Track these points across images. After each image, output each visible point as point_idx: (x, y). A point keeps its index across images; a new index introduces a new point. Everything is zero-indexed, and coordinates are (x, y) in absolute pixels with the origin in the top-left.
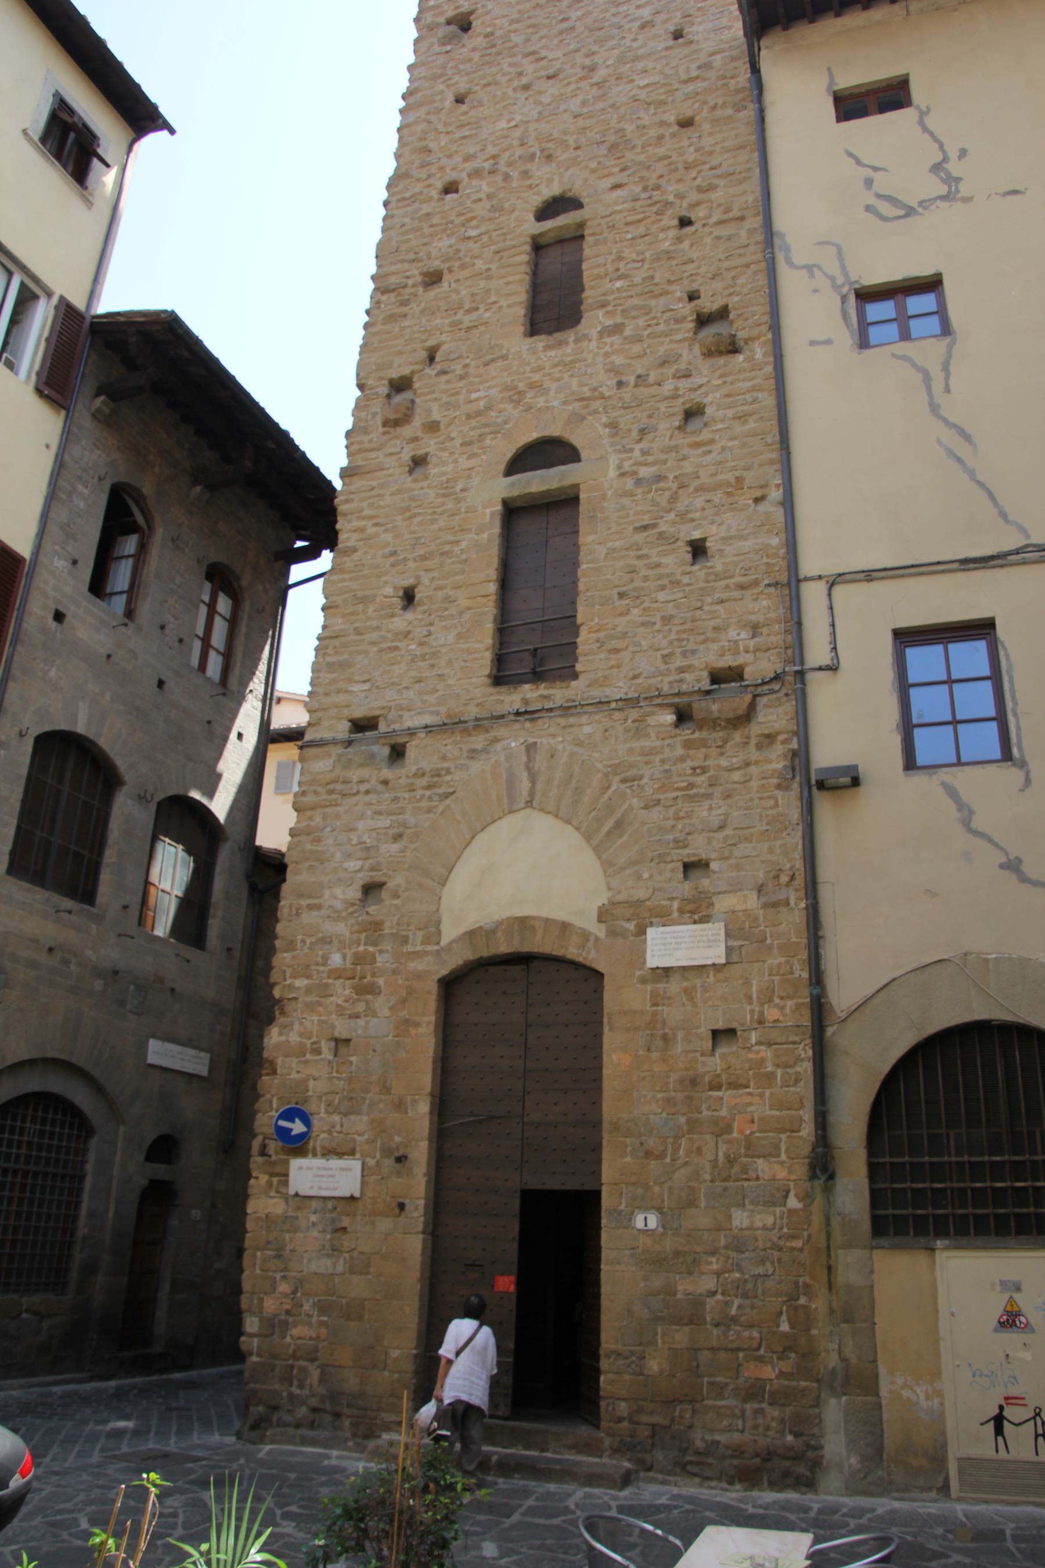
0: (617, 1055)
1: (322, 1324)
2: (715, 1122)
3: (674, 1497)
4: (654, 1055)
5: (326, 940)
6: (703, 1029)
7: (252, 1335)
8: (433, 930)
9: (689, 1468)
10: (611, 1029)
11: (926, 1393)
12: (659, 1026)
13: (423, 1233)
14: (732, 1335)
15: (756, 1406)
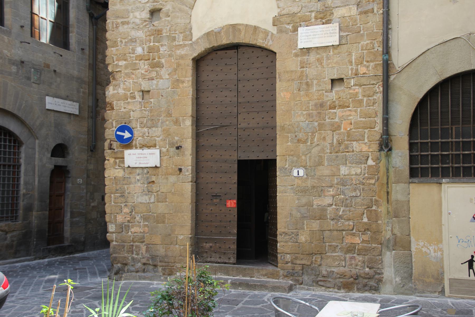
0: (283, 93)
1: (145, 226)
2: (332, 125)
3: (313, 295)
5: (133, 40)
6: (326, 79)
7: (113, 233)
8: (188, 33)
9: (320, 283)
11: (434, 249)
12: (304, 78)
13: (191, 182)
14: (340, 224)
15: (352, 255)
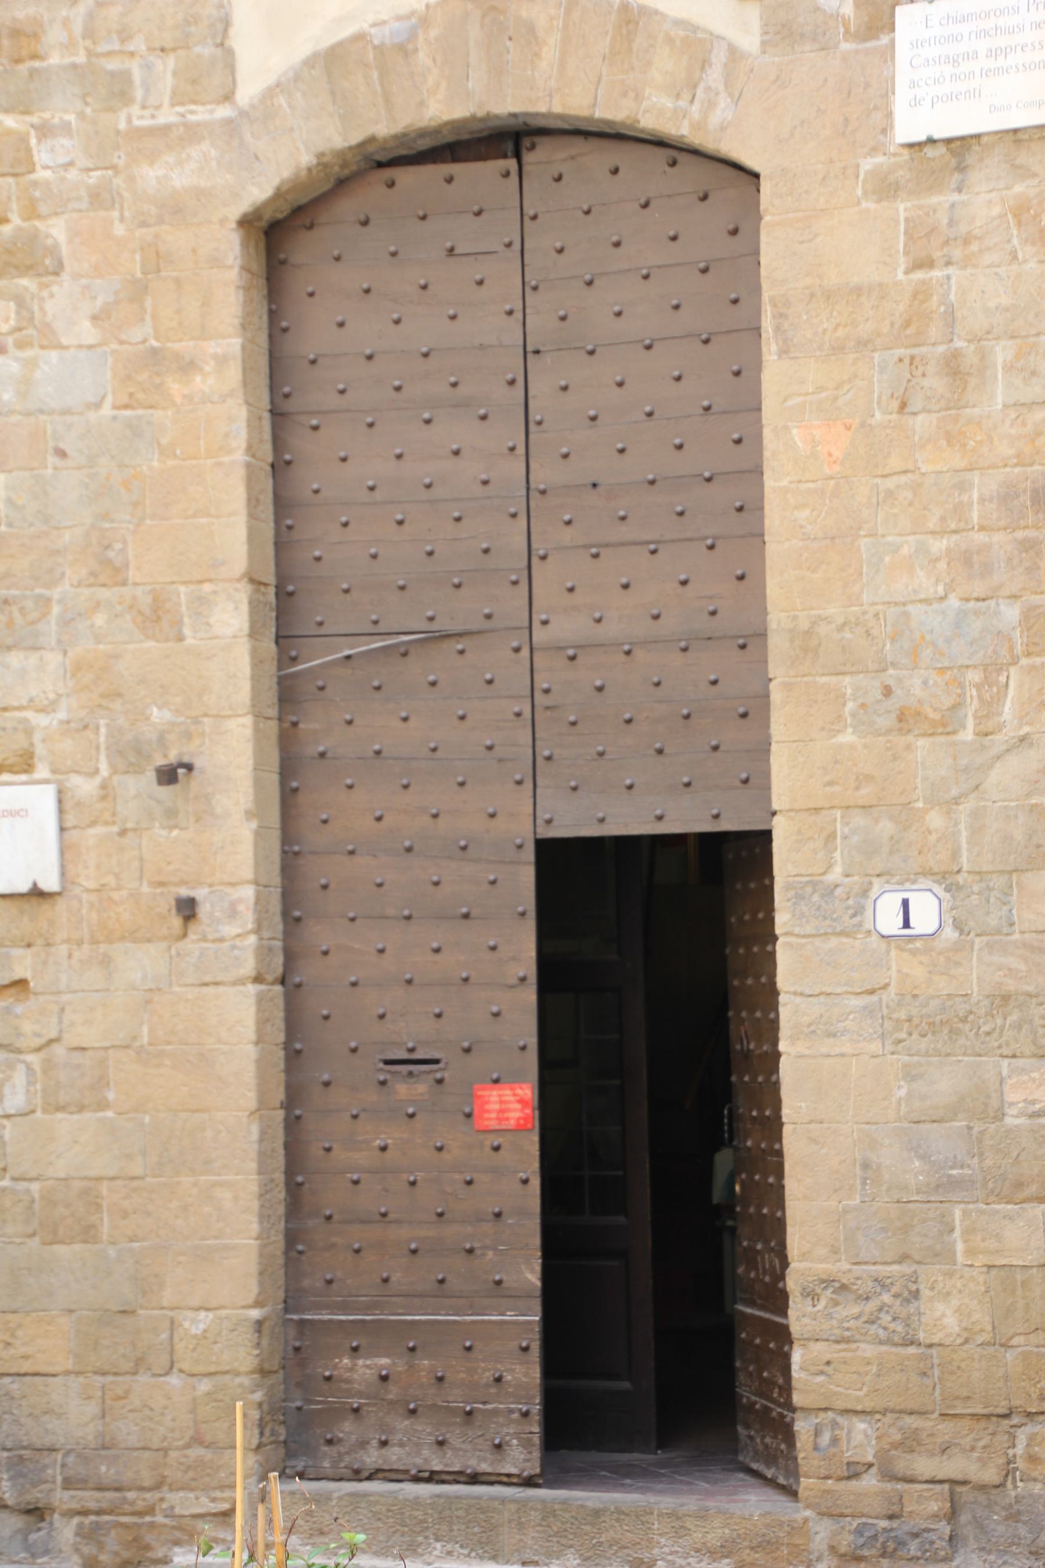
4: (921, 424)
8: (206, 51)
10: (783, 352)
12: (934, 332)
